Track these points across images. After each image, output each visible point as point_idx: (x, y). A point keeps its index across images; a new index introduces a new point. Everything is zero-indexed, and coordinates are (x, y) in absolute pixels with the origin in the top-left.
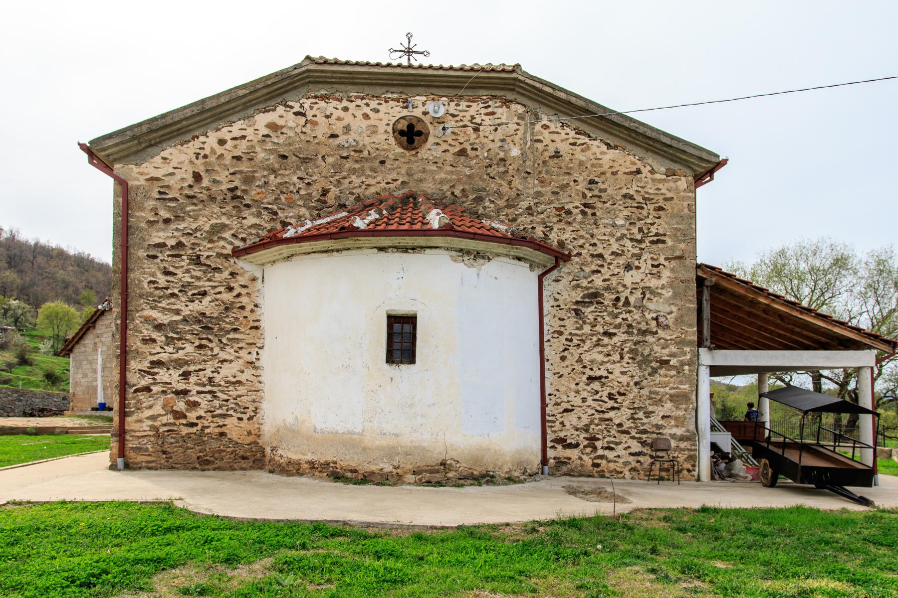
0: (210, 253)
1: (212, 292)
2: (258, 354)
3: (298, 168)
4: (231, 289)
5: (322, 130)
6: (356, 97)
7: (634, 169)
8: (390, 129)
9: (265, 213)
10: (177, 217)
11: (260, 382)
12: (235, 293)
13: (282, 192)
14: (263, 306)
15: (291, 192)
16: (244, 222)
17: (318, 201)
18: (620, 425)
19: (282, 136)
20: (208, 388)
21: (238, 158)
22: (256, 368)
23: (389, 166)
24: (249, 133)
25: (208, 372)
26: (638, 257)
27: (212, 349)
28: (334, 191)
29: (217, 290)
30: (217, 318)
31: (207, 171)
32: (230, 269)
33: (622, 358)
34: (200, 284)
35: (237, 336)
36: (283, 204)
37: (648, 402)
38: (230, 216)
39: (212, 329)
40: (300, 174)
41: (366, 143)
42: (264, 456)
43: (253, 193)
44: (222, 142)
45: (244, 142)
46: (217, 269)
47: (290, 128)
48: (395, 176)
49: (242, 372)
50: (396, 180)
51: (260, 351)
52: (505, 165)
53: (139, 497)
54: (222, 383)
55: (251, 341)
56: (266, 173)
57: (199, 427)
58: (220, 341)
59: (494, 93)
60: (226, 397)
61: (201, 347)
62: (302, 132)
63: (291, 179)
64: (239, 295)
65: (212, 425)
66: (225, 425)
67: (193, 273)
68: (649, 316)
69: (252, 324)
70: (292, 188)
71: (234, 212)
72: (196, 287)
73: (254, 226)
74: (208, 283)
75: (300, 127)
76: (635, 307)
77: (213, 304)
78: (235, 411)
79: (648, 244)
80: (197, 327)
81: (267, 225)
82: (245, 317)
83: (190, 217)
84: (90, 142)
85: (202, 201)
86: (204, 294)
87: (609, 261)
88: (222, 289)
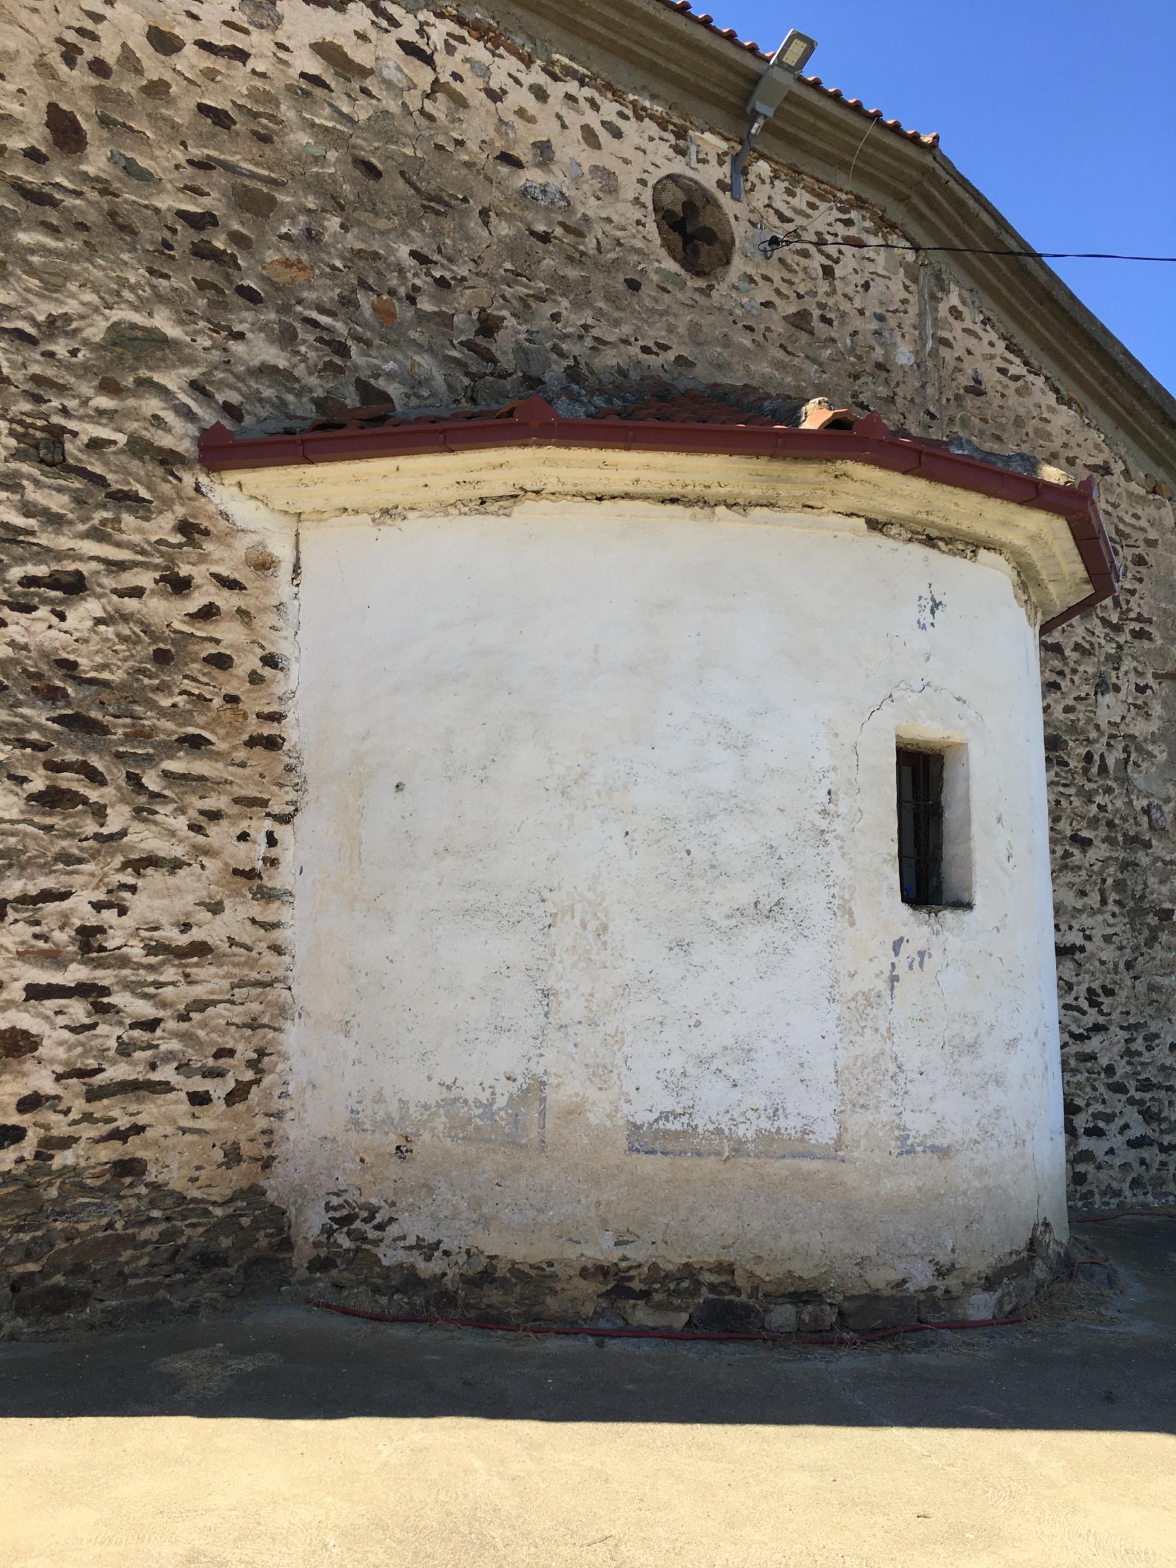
0: (105, 433)
1: (109, 582)
2: (272, 841)
3: (413, 220)
4: (180, 586)
5: (477, 127)
6: (573, 74)
7: (1099, 461)
8: (647, 197)
9: (306, 335)
11: (277, 949)
12: (195, 603)
13: (363, 284)
14: (294, 669)
15: (392, 292)
16: (236, 347)
17: (468, 345)
18: (1110, 1070)
19: (362, 101)
20: (76, 974)
21: (220, 118)
22: (267, 896)
23: (648, 302)
25: (80, 908)
26: (1115, 661)
27: (99, 812)
28: (512, 330)
29: (131, 579)
30: (122, 686)
31: (105, 121)
32: (180, 511)
33: (1104, 902)
34: (64, 542)
35: (201, 767)
36: (365, 325)
37: (1149, 1010)
38: (186, 316)
39: (104, 730)
40: (419, 242)
41: (591, 213)
42: (287, 1244)
43: (271, 256)
45: (240, 71)
46: (125, 499)
47: (388, 84)
48: (663, 337)
49: (216, 908)
50: (665, 348)
51: (281, 831)
52: (887, 382)
54: (136, 951)
55: (251, 792)
56: (311, 203)
57: (28, 1147)
58: (134, 780)
59: (867, 193)
60: (145, 1009)
61: (53, 799)
62: (422, 111)
63: (391, 251)
64: (208, 613)
65: (88, 1132)
66: (138, 1129)
67: (32, 494)
68: (1140, 803)
69: (254, 727)
70: (393, 280)
71: (202, 302)
72: (46, 554)
73: (266, 371)
74: (90, 547)
75: (417, 93)
76: (1116, 780)
77: (107, 631)
78: (183, 1068)
79: (1129, 638)
80: (39, 714)
81: (313, 381)
82: (232, 699)
83: (32, 271)
85: (82, 226)
86: (75, 586)
87: (1072, 664)
88: (146, 579)
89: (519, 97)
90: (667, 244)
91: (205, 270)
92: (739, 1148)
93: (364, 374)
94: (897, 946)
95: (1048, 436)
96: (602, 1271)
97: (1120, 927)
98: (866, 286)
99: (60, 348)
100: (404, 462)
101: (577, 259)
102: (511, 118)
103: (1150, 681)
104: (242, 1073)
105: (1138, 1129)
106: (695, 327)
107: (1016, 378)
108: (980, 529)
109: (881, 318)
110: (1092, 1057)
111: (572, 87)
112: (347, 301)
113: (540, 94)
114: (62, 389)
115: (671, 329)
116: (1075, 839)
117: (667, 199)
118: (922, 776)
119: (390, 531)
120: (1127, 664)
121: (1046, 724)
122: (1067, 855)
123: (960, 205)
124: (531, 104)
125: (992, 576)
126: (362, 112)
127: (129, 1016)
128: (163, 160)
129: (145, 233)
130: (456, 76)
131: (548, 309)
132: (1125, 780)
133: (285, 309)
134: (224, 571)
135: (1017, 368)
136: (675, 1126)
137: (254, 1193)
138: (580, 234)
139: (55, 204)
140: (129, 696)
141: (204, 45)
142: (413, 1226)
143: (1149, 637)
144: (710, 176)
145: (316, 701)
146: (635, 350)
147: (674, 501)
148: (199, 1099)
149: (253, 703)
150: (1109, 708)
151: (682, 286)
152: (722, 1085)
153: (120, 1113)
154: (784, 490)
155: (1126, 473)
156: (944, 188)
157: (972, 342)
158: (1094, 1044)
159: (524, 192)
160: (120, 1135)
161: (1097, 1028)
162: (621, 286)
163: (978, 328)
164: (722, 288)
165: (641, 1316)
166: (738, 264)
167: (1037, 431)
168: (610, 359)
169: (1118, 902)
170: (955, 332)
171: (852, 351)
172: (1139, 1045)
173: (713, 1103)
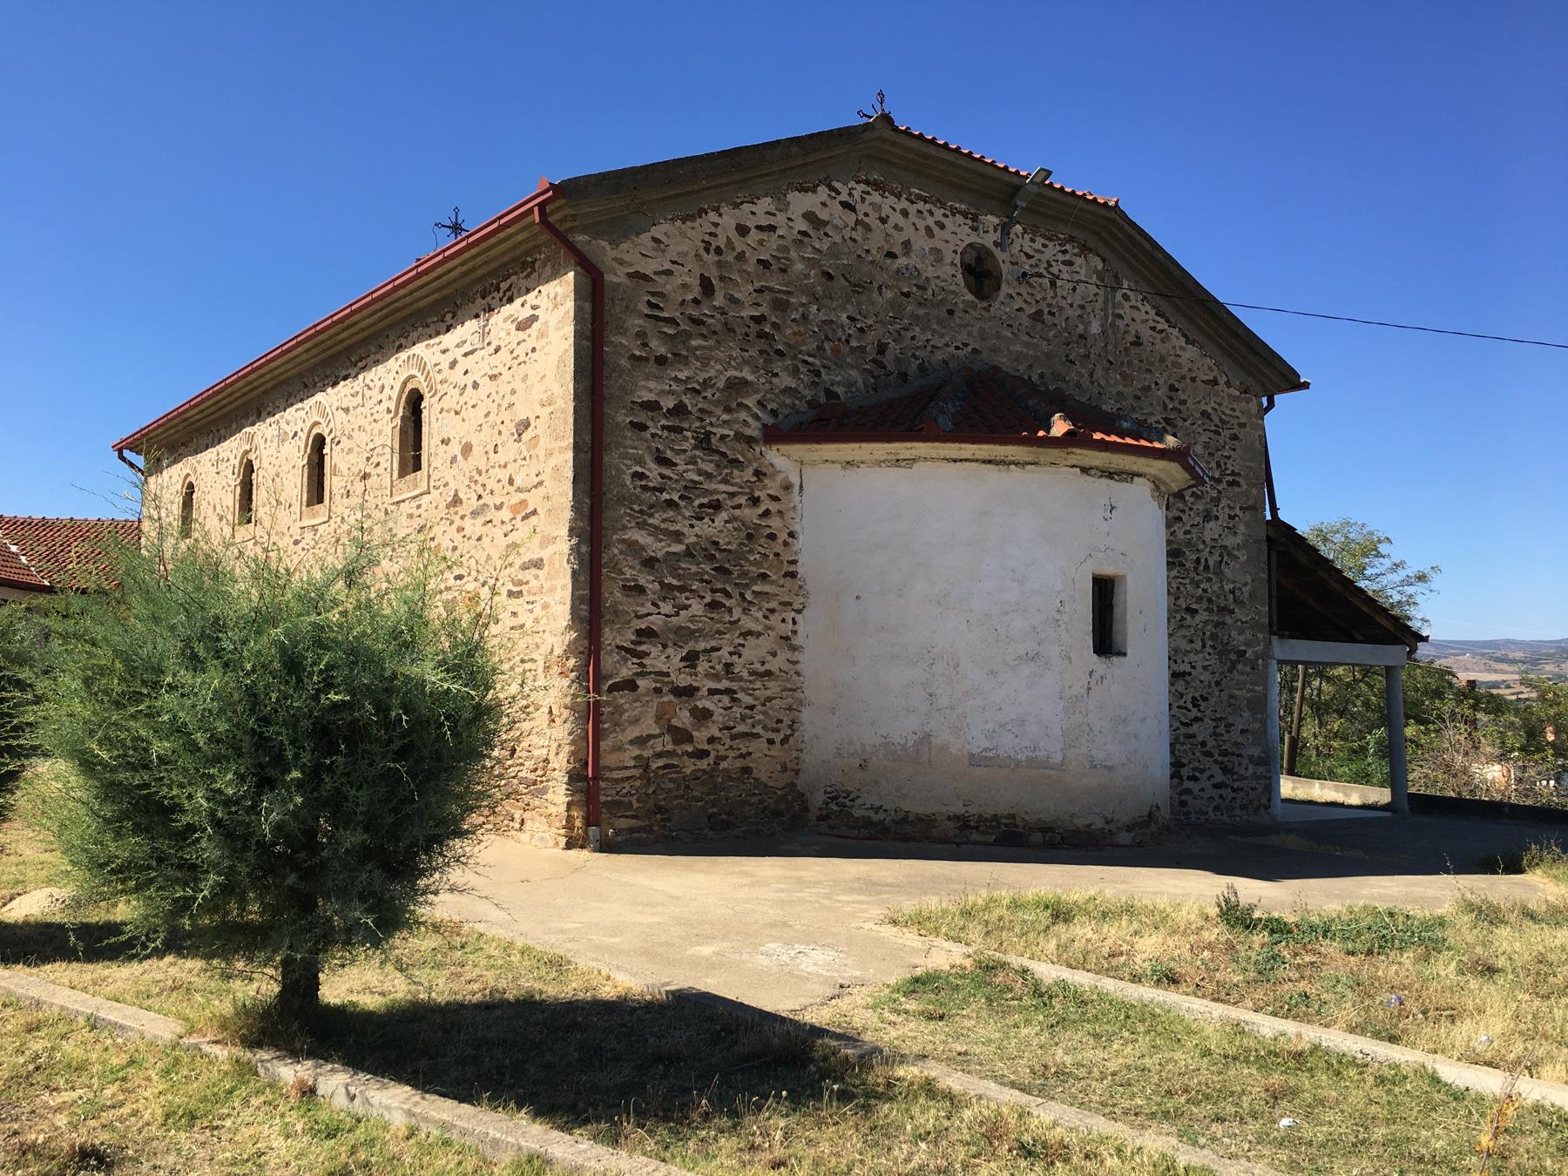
0: (726, 432)
1: (730, 503)
2: (794, 622)
3: (848, 300)
4: (755, 501)
5: (876, 242)
9: (803, 369)
11: (798, 674)
13: (827, 338)
16: (775, 380)
17: (874, 361)
18: (1203, 744)
19: (826, 240)
20: (724, 684)
22: (794, 648)
26: (1216, 501)
27: (730, 611)
33: (1204, 646)
34: (713, 486)
35: (766, 588)
37: (1229, 710)
40: (851, 310)
42: (806, 809)
46: (734, 462)
47: (836, 227)
50: (966, 345)
51: (799, 618)
54: (745, 674)
57: (711, 759)
58: (742, 595)
60: (749, 700)
61: (714, 606)
64: (767, 513)
65: (732, 754)
73: (787, 390)
74: (723, 487)
80: (707, 567)
81: (806, 392)
82: (777, 555)
83: (697, 359)
85: (715, 333)
89: (896, 218)
90: (967, 285)
91: (762, 344)
92: (1018, 764)
93: (828, 385)
94: (1091, 673)
95: (1180, 366)
96: (957, 817)
97: (1213, 661)
98: (1074, 289)
99: (708, 394)
100: (864, 445)
101: (922, 304)
102: (891, 231)
103: (1238, 511)
104: (786, 731)
105: (1219, 778)
106: (982, 330)
107: (1161, 332)
108: (1135, 468)
109: (1082, 307)
110: (1193, 736)
111: (920, 205)
112: (820, 348)
113: (905, 213)
114: (710, 413)
115: (969, 334)
116: (1188, 609)
117: (967, 257)
119: (851, 472)
120: (1224, 502)
121: (1169, 542)
122: (1183, 619)
123: (1130, 237)
124: (901, 221)
125: (1142, 488)
126: (824, 246)
128: (744, 292)
129: (738, 331)
130: (866, 215)
131: (909, 334)
132: (1219, 574)
133: (794, 358)
134: (772, 492)
135: (1162, 325)
136: (990, 754)
137: (792, 785)
138: (925, 289)
139: (703, 323)
140: (738, 556)
141: (759, 228)
142: (870, 799)
143: (1238, 484)
144: (989, 240)
145: (810, 552)
146: (951, 349)
147: (990, 462)
148: (771, 742)
149: (785, 557)
150: (1212, 530)
151: (975, 307)
152: (1011, 736)
153: (743, 746)
154: (1042, 459)
155: (1228, 384)
156: (1121, 228)
157: (1135, 314)
158: (1195, 728)
159: (898, 271)
160: (742, 756)
161: (1197, 719)
162: (945, 315)
163: (1139, 305)
164: (996, 304)
165: (975, 836)
166: (1005, 289)
167: (1172, 363)
168: (939, 356)
169: (1212, 647)
170: (1126, 311)
171: (1066, 330)
172: (1222, 729)
173: (1007, 744)
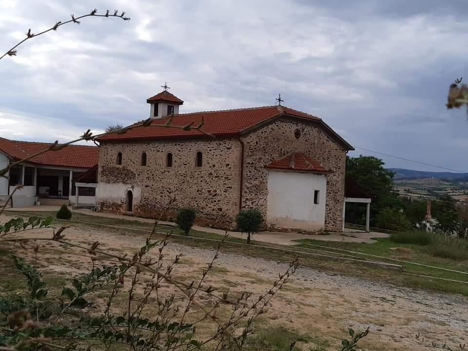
10: (253, 155)
24: (267, 130)
44: (262, 133)
53: (382, 237)
61: (256, 194)
73: (268, 158)
84: (352, 159)
118: (316, 192)
127: (6, 177)
